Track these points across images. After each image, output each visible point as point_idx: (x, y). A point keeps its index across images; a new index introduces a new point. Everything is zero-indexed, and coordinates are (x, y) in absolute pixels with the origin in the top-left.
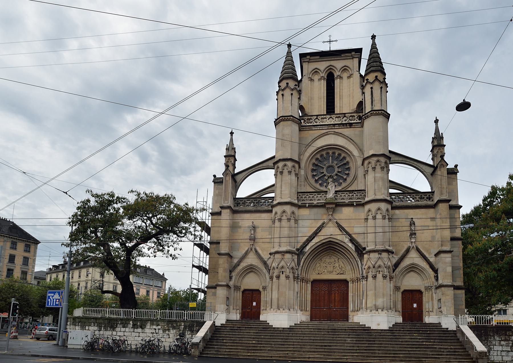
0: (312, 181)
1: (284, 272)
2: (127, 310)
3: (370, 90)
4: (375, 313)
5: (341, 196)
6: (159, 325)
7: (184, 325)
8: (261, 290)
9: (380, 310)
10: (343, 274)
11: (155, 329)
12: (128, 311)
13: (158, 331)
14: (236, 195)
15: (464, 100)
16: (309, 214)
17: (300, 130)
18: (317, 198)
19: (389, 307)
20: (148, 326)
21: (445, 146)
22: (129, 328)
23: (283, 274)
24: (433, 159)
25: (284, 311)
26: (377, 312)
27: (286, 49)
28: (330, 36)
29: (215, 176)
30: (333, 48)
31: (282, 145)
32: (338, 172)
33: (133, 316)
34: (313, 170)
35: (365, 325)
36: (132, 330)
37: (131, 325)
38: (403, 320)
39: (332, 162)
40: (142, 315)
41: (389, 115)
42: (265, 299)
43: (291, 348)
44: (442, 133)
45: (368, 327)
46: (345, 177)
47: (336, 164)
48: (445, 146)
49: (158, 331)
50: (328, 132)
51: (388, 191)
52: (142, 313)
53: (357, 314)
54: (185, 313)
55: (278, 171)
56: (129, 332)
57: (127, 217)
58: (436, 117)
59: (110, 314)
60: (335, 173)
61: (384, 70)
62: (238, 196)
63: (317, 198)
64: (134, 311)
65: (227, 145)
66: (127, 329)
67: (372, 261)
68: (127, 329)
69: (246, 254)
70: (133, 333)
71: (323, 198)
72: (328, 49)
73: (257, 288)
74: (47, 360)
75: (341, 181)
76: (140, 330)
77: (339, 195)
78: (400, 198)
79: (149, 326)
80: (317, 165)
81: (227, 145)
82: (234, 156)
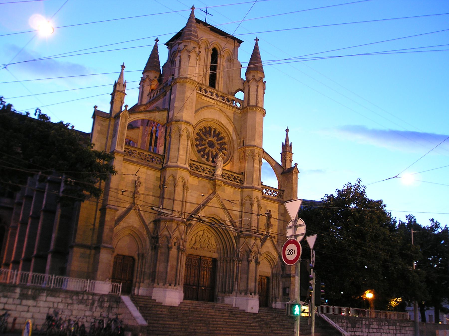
7: (92, 299)
8: (136, 257)
19: (254, 290)
20: (43, 297)
25: (175, 287)
26: (251, 296)
33: (333, 313)
36: (18, 302)
37: (17, 296)
38: (261, 305)
42: (143, 270)
44: (291, 143)
45: (160, 303)
47: (205, 140)
53: (229, 296)
54: (52, 278)
56: (14, 304)
57: (330, 214)
59: (57, 284)
64: (53, 277)
65: (283, 143)
66: (10, 301)
70: (19, 306)
76: (30, 302)
81: (283, 143)
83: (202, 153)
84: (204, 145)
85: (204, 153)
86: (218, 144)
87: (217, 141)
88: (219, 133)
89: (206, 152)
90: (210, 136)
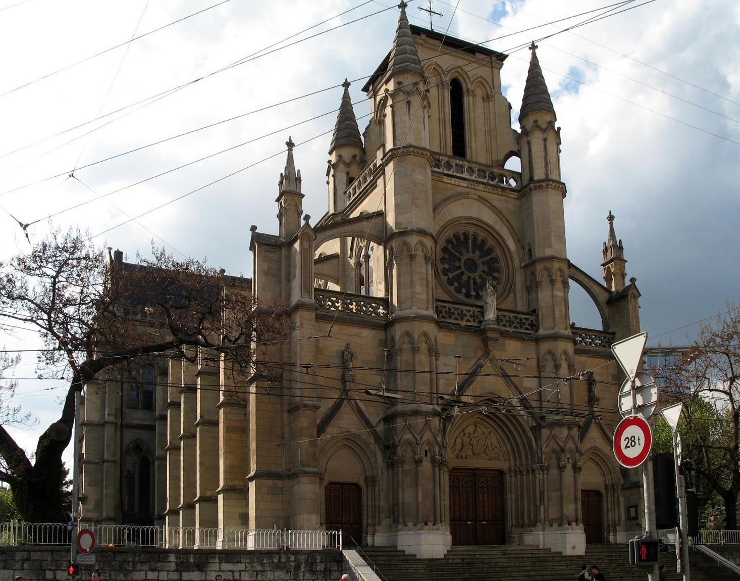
1: (428, 453)
2: (48, 525)
3: (542, 143)
4: (568, 529)
6: (241, 563)
8: (362, 484)
9: (574, 524)
11: (233, 572)
12: (40, 527)
13: (240, 575)
16: (454, 344)
21: (303, 196)
22: (168, 571)
23: (426, 455)
25: (435, 527)
27: (529, 53)
29: (253, 228)
31: (413, 202)
35: (550, 549)
37: (173, 566)
38: (589, 541)
40: (60, 535)
48: (303, 196)
49: (240, 575)
52: (698, 541)
58: (290, 137)
67: (415, 432)
68: (161, 573)
69: (337, 408)
73: (354, 480)
75: (464, 291)
79: (218, 564)
81: (605, 243)
83: (456, 284)
84: (459, 268)
85: (460, 284)
86: (484, 263)
87: (481, 257)
89: (462, 282)
90: (459, 260)
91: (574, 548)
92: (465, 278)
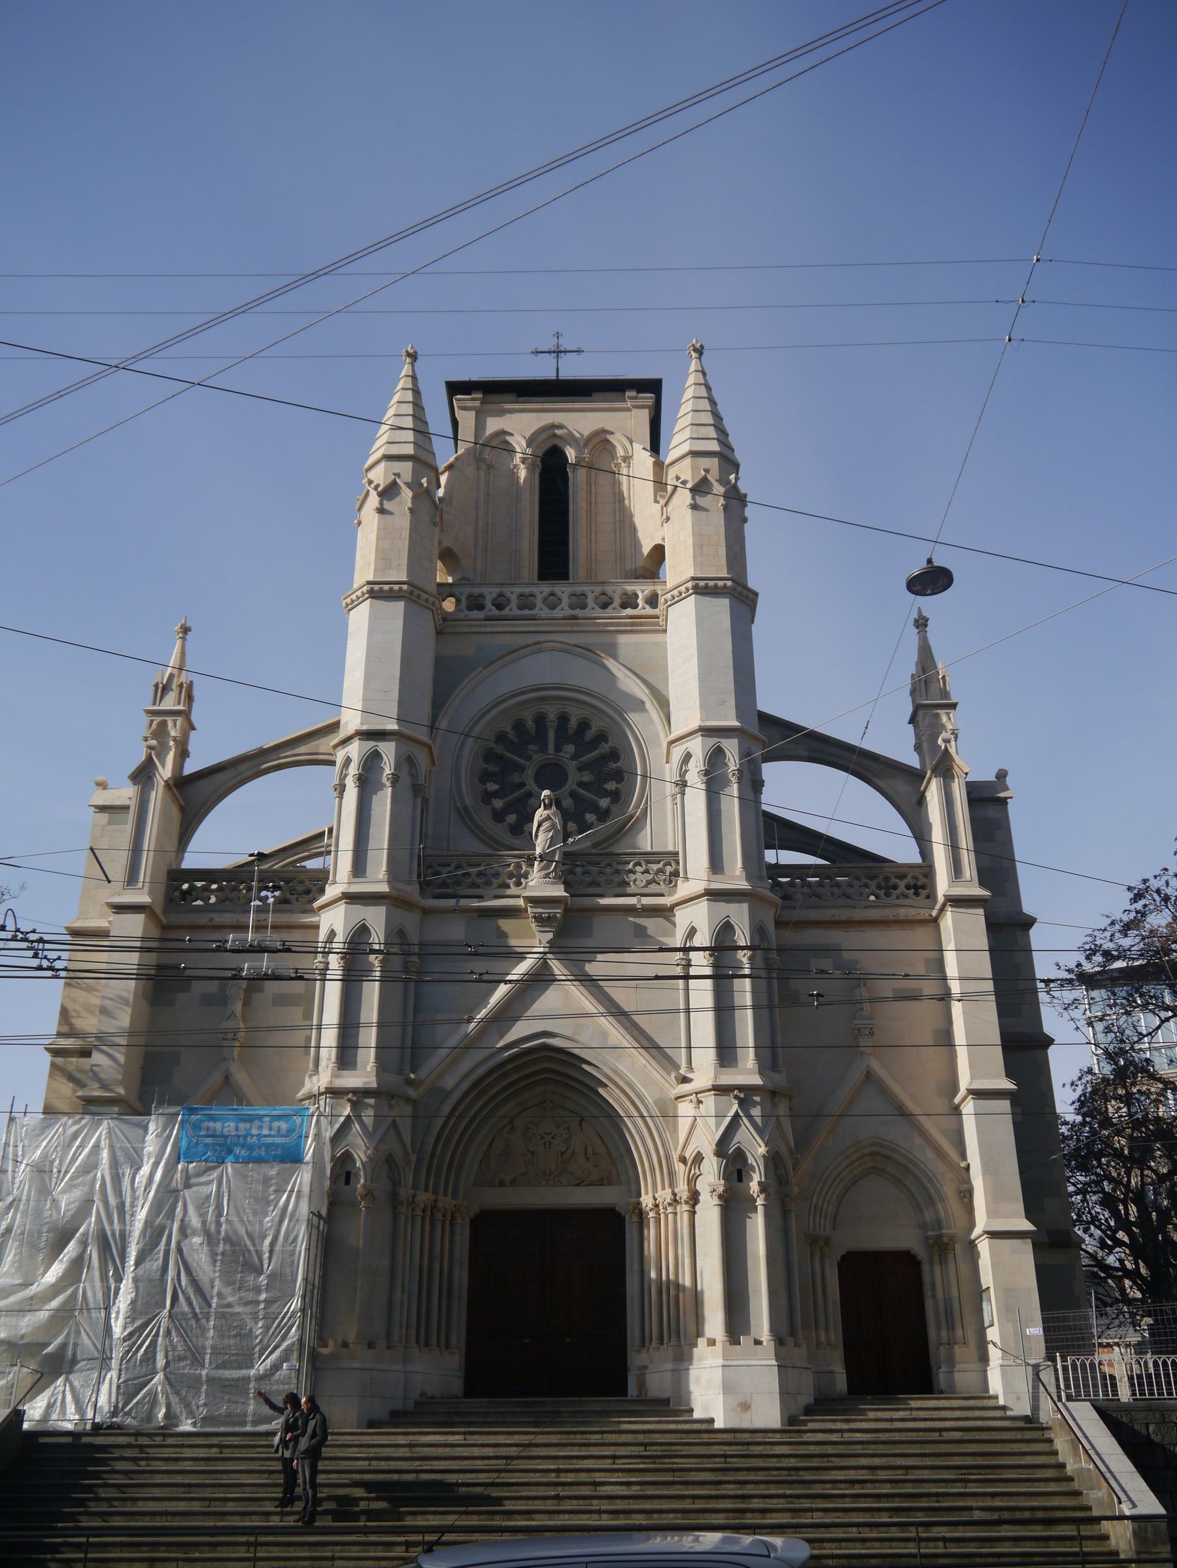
0: (484, 817)
5: (588, 872)
10: (600, 1182)
14: (182, 859)
15: (929, 561)
17: (439, 633)
18: (588, 879)
24: (918, 748)
28: (558, 335)
30: (566, 374)
32: (581, 784)
34: (485, 777)
39: (558, 749)
41: (756, 594)
43: (561, 1516)
46: (604, 803)
50: (539, 643)
51: (761, 857)
55: (346, 775)
60: (567, 786)
61: (733, 450)
62: (192, 861)
63: (588, 879)
71: (638, 875)
72: (550, 374)
74: (239, 1564)
77: (579, 870)
78: (838, 885)
80: (500, 758)
82: (186, 714)
86: (529, 758)
88: (519, 726)
91: (745, 1406)
92: (587, 777)
